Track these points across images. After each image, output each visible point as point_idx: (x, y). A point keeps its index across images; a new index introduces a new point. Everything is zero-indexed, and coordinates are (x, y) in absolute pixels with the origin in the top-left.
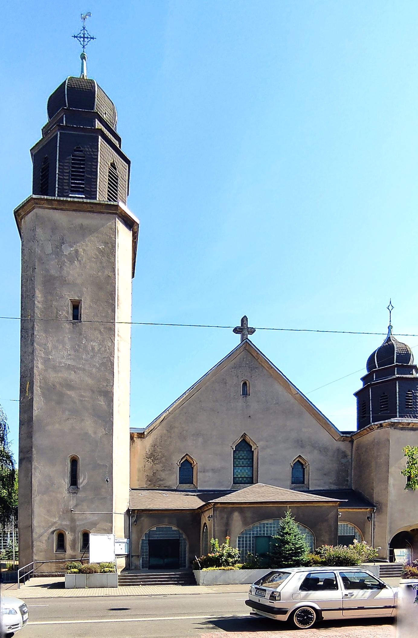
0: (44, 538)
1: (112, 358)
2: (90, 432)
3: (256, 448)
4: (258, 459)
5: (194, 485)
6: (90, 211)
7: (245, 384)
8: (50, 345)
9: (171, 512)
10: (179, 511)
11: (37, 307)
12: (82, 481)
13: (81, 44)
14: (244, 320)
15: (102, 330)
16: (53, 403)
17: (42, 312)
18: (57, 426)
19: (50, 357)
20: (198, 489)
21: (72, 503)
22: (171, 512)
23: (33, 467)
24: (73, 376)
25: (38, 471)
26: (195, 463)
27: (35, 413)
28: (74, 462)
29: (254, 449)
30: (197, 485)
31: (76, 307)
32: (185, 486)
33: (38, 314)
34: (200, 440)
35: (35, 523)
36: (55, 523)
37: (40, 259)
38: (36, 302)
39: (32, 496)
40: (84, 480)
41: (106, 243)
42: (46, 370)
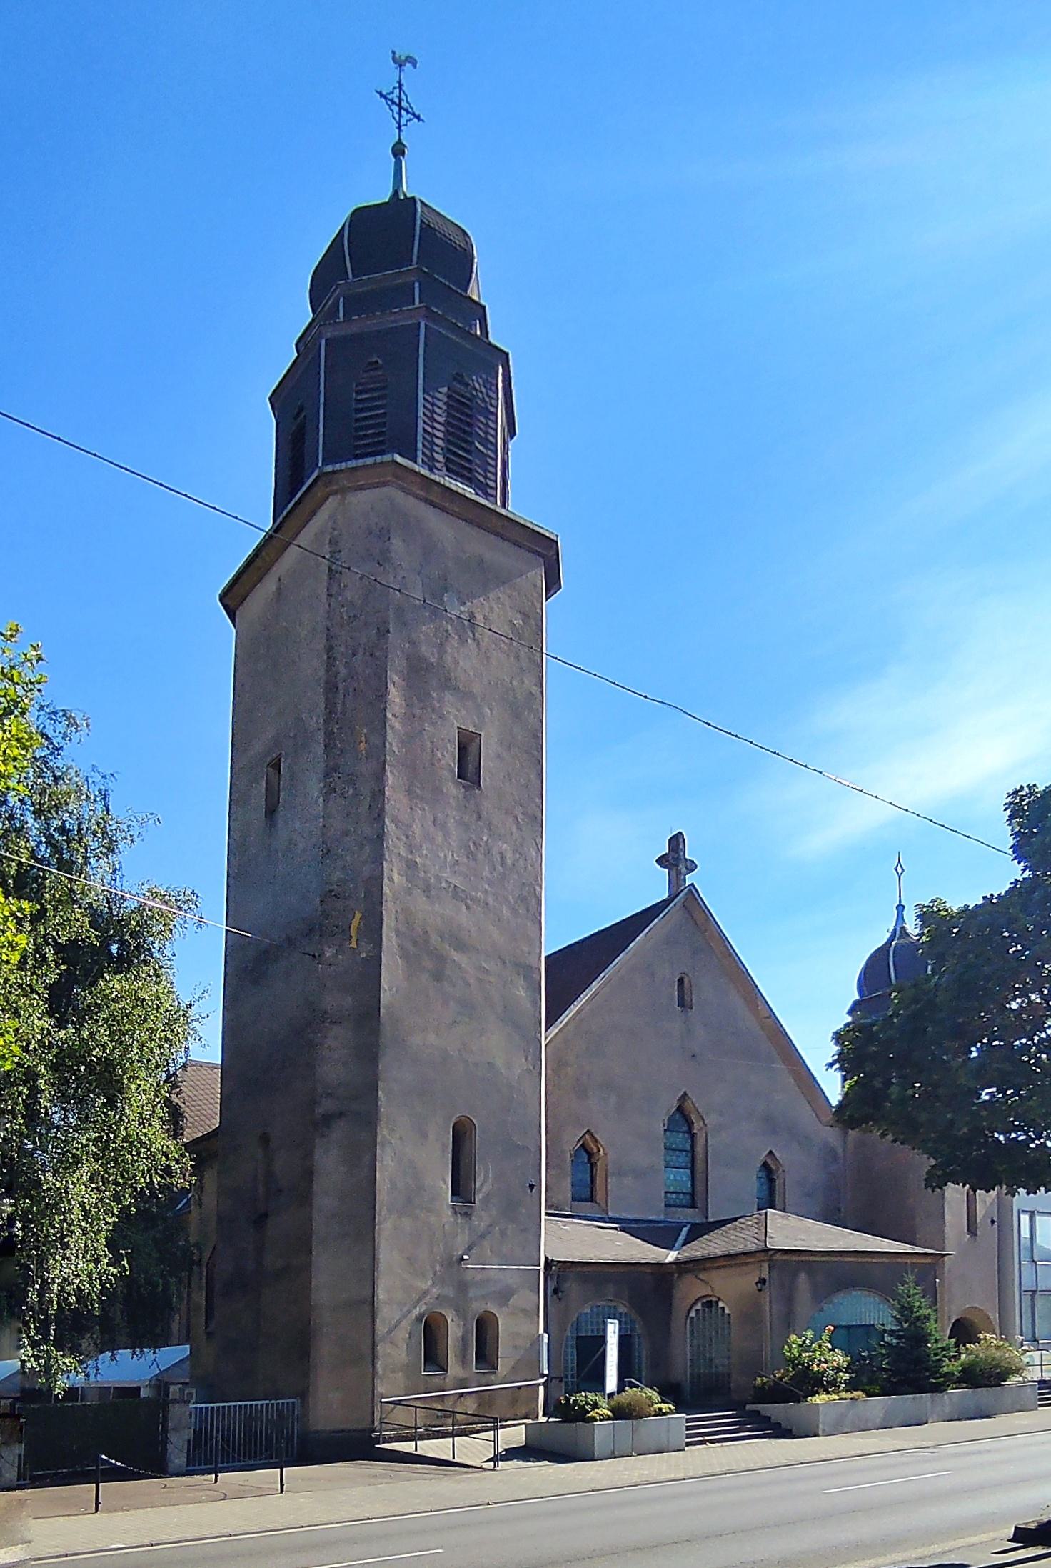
0: (402, 1334)
1: (538, 888)
2: (499, 1062)
3: (701, 1129)
4: (707, 1153)
5: (599, 1204)
6: (497, 534)
7: (681, 981)
8: (417, 829)
9: (622, 1269)
10: (611, 1270)
11: (392, 727)
12: (483, 1183)
13: (394, 118)
14: (676, 841)
15: (520, 817)
16: (425, 977)
17: (402, 742)
18: (432, 1038)
19: (418, 860)
20: (610, 1214)
21: (461, 1241)
22: (622, 1269)
23: (378, 1140)
24: (463, 917)
25: (388, 1150)
26: (601, 1152)
27: (385, 998)
28: (461, 1136)
29: (698, 1130)
30: (607, 1206)
31: (467, 747)
32: (586, 1207)
33: (394, 744)
34: (613, 1099)
35: (381, 1294)
36: (425, 1293)
37: (400, 612)
38: (389, 715)
39: (375, 1218)
40: (484, 1182)
41: (525, 616)
42: (409, 891)
